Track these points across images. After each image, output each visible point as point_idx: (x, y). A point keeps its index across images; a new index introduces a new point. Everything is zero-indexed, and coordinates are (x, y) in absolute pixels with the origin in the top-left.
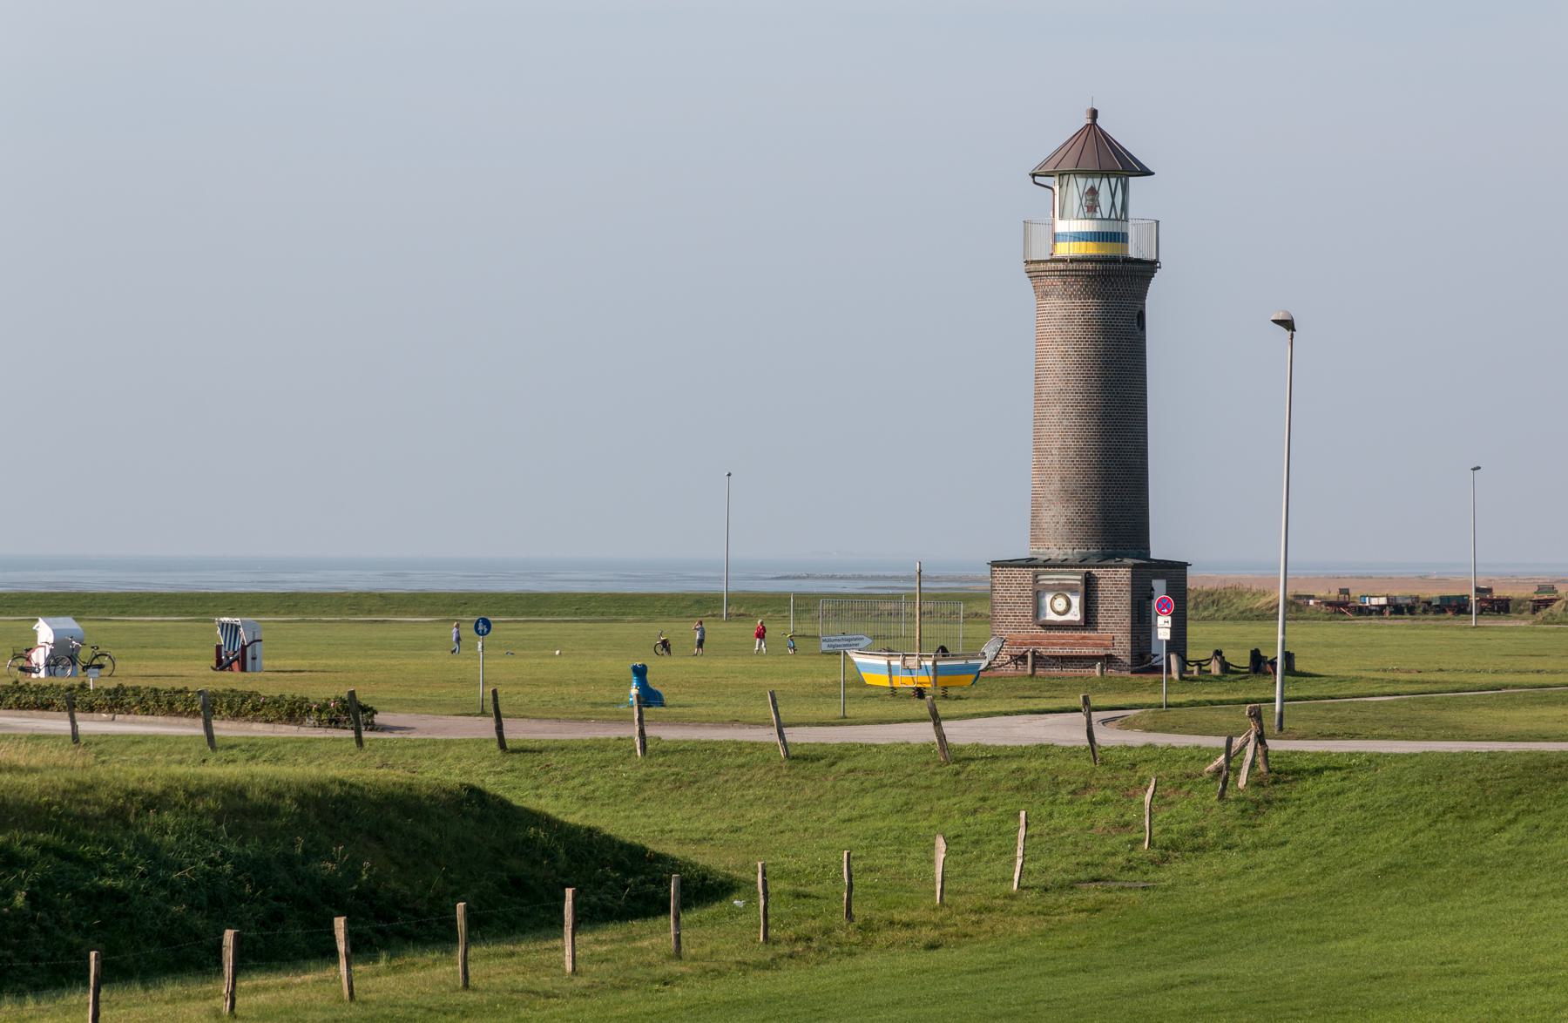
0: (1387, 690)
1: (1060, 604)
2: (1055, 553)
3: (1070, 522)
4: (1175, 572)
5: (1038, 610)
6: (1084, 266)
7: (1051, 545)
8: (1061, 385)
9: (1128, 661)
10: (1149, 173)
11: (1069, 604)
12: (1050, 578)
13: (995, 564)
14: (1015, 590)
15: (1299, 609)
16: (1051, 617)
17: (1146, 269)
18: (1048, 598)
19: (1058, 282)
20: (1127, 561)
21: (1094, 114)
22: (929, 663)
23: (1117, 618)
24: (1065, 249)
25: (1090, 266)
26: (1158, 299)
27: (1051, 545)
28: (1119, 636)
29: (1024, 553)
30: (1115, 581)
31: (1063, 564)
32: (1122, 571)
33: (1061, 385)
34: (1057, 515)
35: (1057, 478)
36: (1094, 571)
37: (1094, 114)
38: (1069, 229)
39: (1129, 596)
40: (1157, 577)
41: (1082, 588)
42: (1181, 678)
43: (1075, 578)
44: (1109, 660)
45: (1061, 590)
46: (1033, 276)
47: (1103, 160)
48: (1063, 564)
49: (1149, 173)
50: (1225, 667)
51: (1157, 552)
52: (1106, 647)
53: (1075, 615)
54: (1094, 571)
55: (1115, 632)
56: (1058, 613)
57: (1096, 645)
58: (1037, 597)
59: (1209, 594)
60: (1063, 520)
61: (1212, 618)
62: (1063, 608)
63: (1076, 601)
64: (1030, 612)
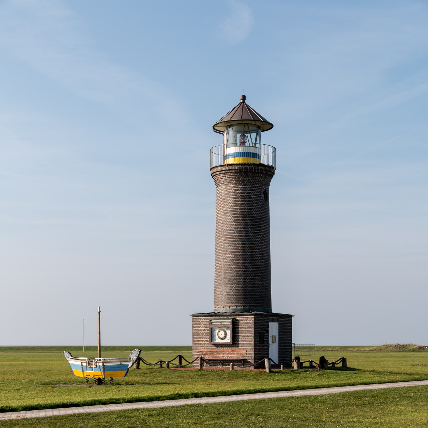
0: (377, 379)
1: (222, 334)
2: (222, 310)
3: (228, 294)
4: (285, 321)
5: (212, 338)
6: (233, 167)
7: (220, 305)
8: (224, 227)
9: (253, 362)
10: (271, 126)
11: (226, 334)
12: (217, 321)
13: (194, 315)
14: (202, 328)
15: (424, 349)
16: (218, 341)
17: (268, 172)
18: (217, 331)
19: (222, 176)
20: (253, 313)
21: (244, 98)
22: (101, 364)
23: (248, 340)
24: (230, 161)
25: (236, 167)
26: (276, 189)
27: (220, 305)
28: (249, 350)
29: (211, 310)
30: (247, 322)
31: (224, 315)
32: (250, 317)
33: (224, 227)
34: (225, 290)
35: (223, 273)
36: (237, 318)
37: (244, 98)
38: (231, 152)
39: (253, 330)
40: (272, 321)
41: (231, 326)
42: (270, 371)
43: (228, 321)
44: (243, 362)
45: (223, 327)
46: (213, 175)
47: (249, 122)
48: (224, 315)
49: (271, 126)
50: (300, 365)
51: (275, 309)
52: (243, 355)
53: (228, 340)
54: (237, 318)
55: (247, 348)
56: (221, 339)
57: (238, 355)
58: (212, 330)
59: (403, 345)
60: (225, 293)
61: (403, 351)
62: (223, 336)
63: (229, 332)
64: (208, 337)
